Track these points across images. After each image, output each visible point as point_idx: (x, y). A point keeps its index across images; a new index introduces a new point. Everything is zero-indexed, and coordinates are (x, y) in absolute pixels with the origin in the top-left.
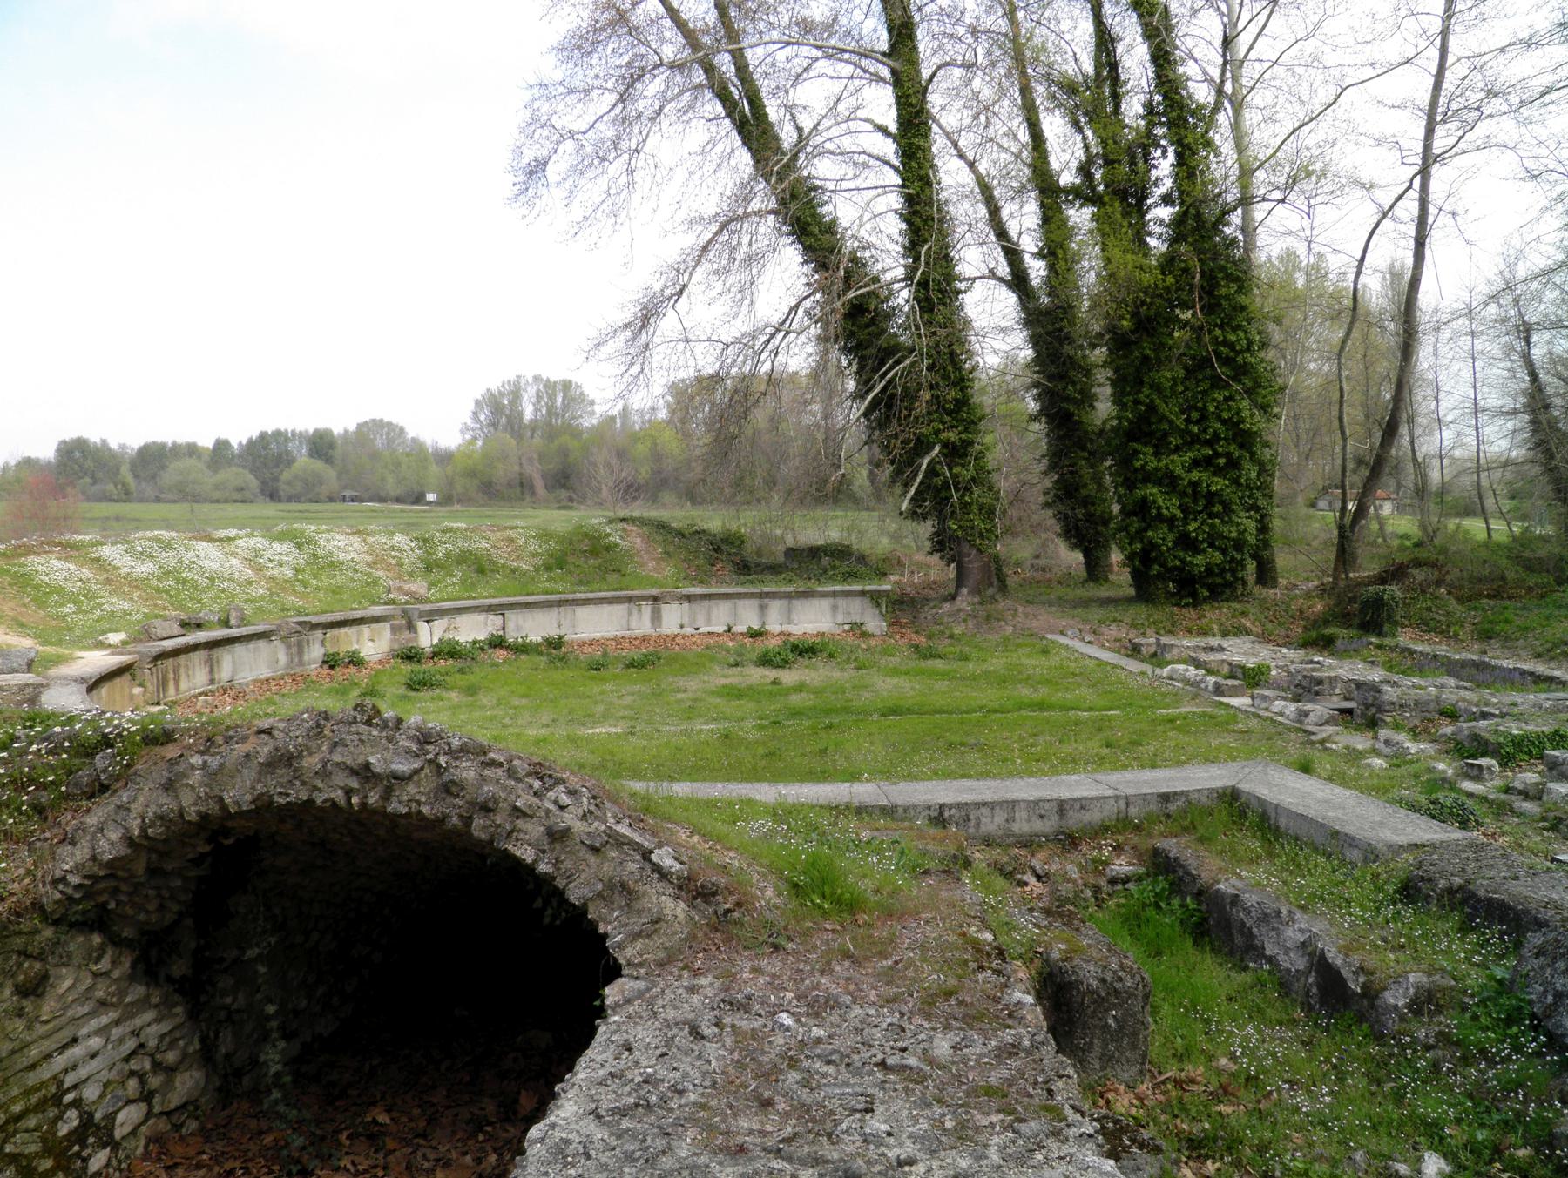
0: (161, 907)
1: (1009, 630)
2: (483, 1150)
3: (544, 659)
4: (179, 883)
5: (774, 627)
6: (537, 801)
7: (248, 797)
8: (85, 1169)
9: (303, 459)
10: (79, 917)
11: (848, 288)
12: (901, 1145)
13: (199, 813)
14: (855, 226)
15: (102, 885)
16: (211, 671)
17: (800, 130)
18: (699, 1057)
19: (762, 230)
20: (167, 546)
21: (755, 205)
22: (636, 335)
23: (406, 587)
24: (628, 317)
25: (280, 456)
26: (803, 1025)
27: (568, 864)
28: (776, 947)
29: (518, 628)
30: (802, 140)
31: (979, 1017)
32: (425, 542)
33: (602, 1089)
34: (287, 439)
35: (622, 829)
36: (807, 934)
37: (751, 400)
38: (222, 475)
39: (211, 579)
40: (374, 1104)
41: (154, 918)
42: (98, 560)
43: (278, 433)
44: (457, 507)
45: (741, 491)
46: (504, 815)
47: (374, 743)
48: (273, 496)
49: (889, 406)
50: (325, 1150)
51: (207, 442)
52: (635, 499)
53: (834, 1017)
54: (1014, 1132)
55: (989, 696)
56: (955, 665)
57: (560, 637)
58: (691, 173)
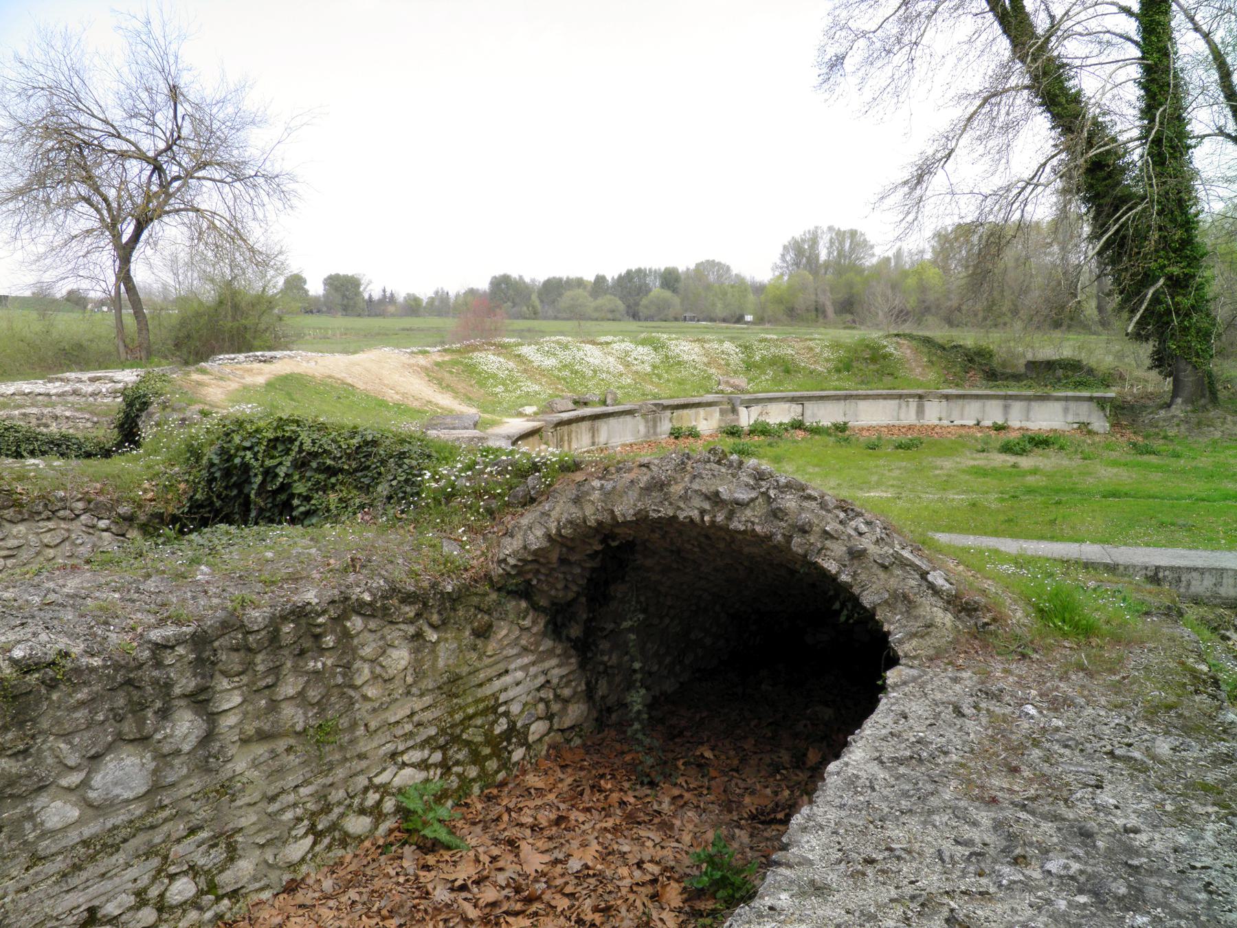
0: (566, 587)
1: (1218, 434)
2: (779, 786)
3: (832, 439)
4: (579, 571)
5: (1015, 423)
6: (841, 527)
7: (631, 511)
8: (509, 759)
9: (656, 290)
10: (514, 588)
11: (1090, 144)
12: (1126, 817)
13: (597, 521)
14: (1098, 96)
15: (529, 567)
16: (593, 436)
17: (1052, 17)
18: (961, 729)
19: (1018, 101)
20: (565, 347)
21: (1013, 81)
22: (913, 189)
23: (732, 381)
24: (907, 176)
25: (640, 288)
26: (1045, 716)
27: (863, 577)
28: (1024, 656)
29: (814, 415)
30: (1054, 26)
31: (1197, 729)
32: (746, 348)
33: (884, 744)
34: (645, 274)
35: (906, 554)
36: (1049, 648)
37: (1004, 241)
38: (600, 301)
39: (595, 371)
40: (702, 744)
41: (561, 594)
42: (519, 356)
43: (639, 271)
44: (767, 326)
45: (991, 316)
46: (817, 536)
47: (722, 477)
48: (635, 316)
49: (1121, 246)
50: (667, 770)
51: (590, 277)
52: (905, 321)
53: (1071, 713)
54: (1229, 823)
55: (1199, 487)
56: (1167, 461)
57: (845, 424)
58: (959, 59)
